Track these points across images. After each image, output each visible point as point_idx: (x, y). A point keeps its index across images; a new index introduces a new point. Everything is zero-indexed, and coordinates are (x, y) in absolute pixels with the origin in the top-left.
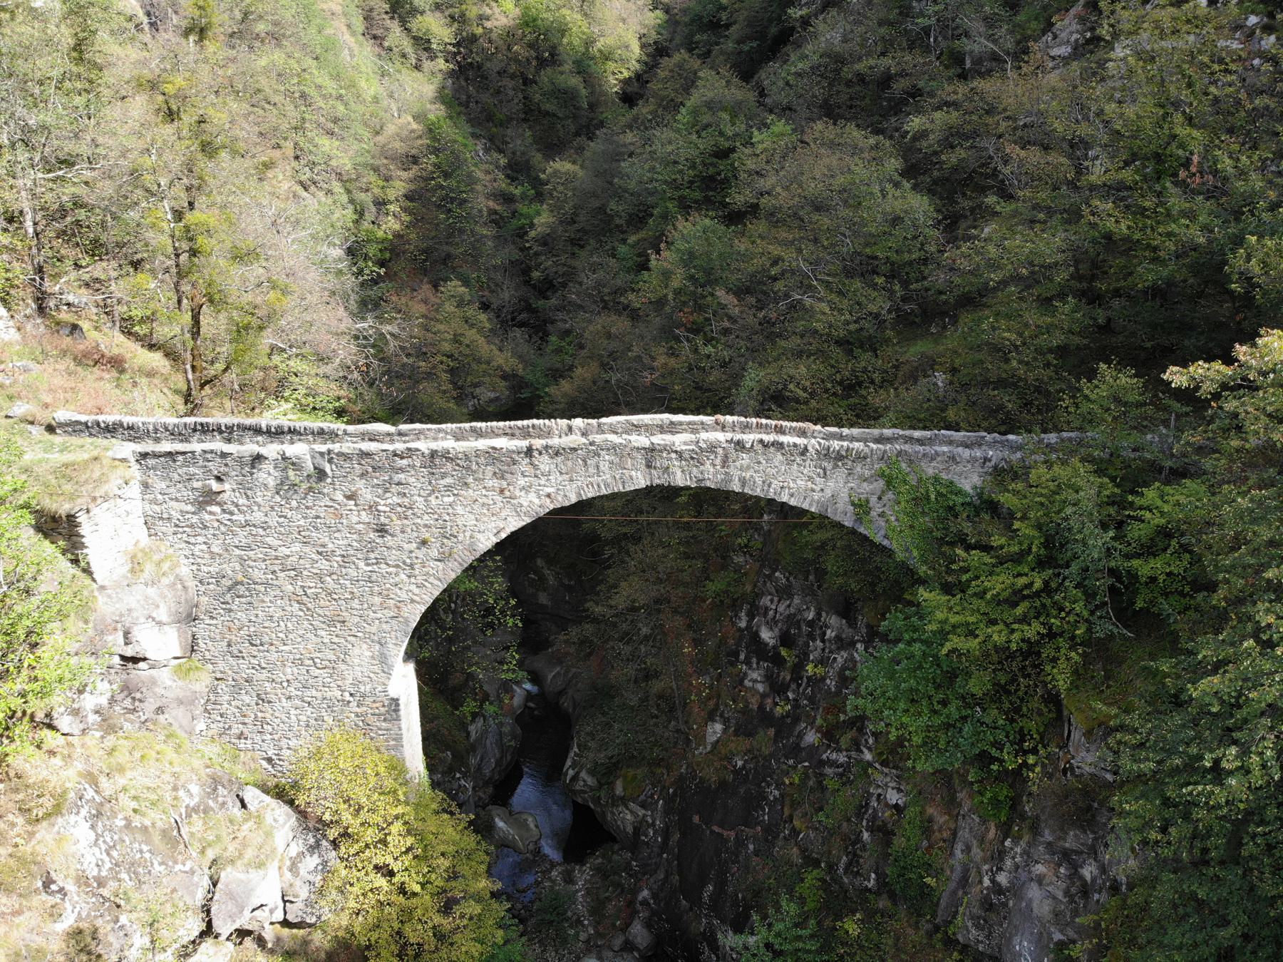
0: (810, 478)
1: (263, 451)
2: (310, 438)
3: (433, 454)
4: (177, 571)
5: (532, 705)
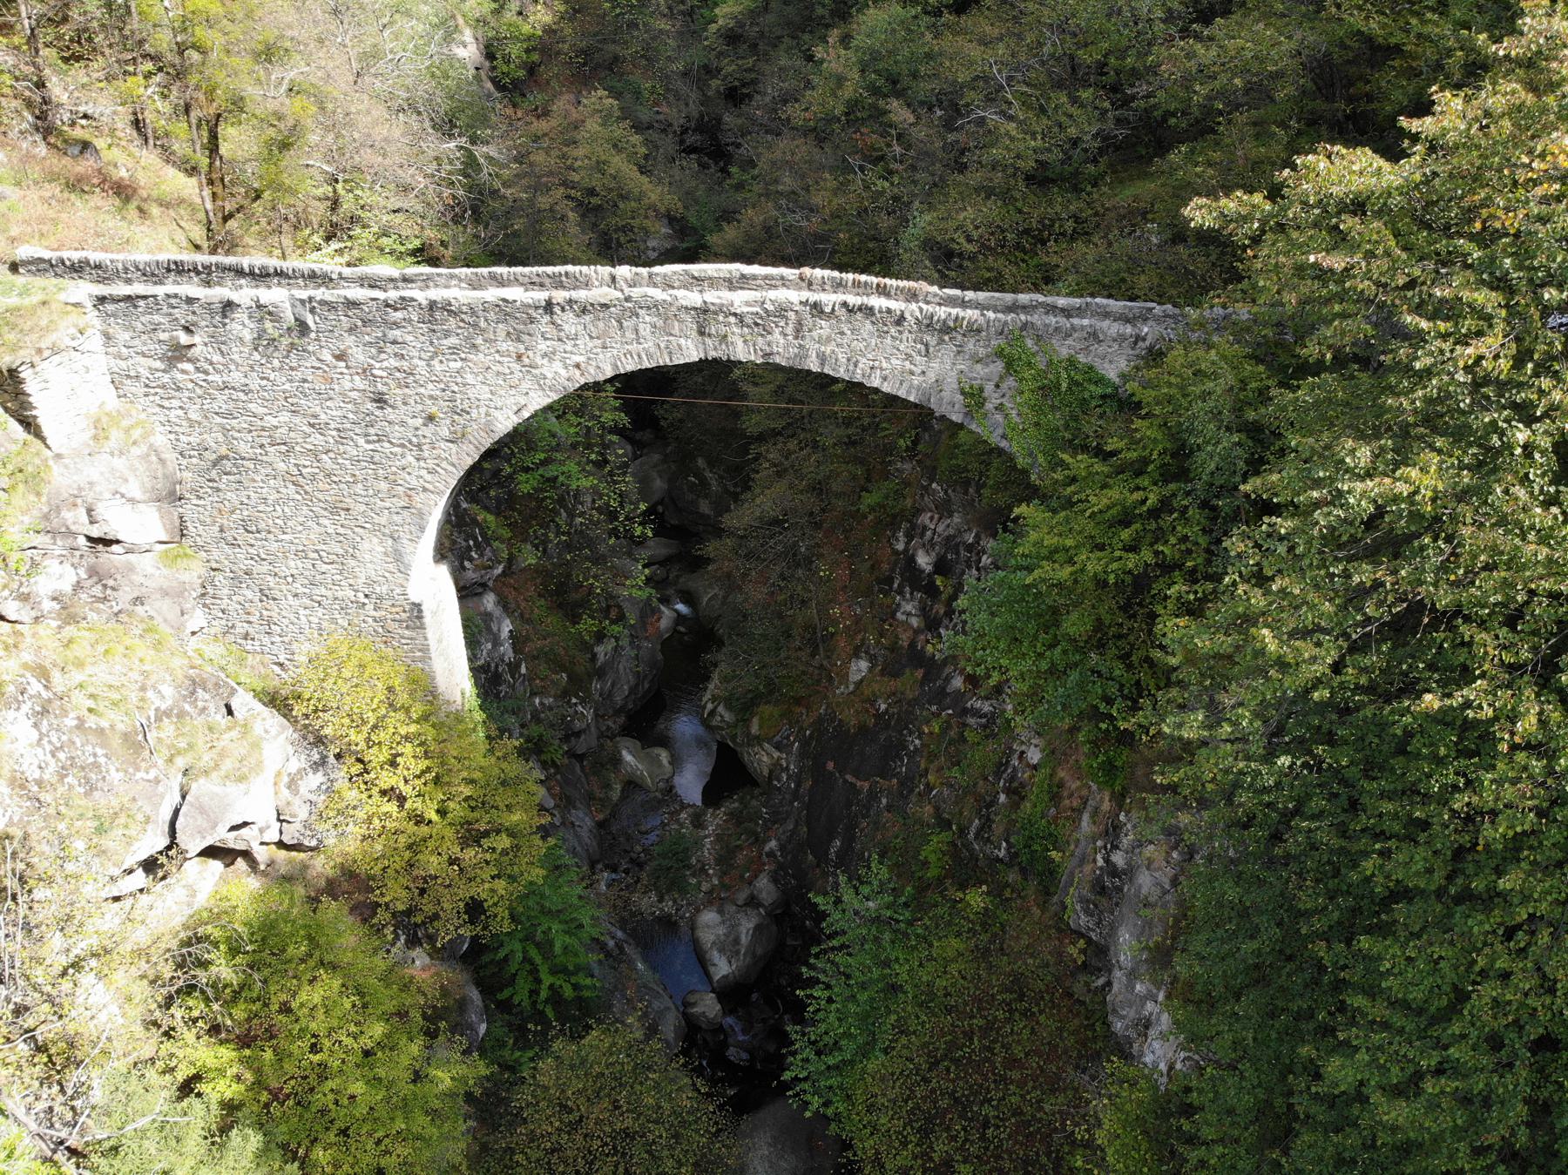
0: (908, 357)
1: (235, 297)
2: (300, 281)
3: (432, 305)
4: (152, 439)
5: (682, 629)
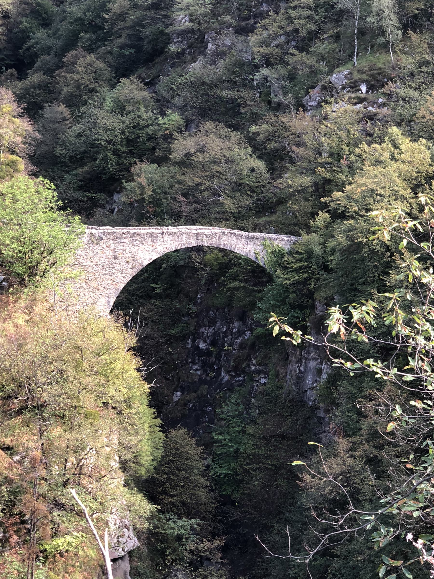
0: (243, 245)
3: (134, 233)
